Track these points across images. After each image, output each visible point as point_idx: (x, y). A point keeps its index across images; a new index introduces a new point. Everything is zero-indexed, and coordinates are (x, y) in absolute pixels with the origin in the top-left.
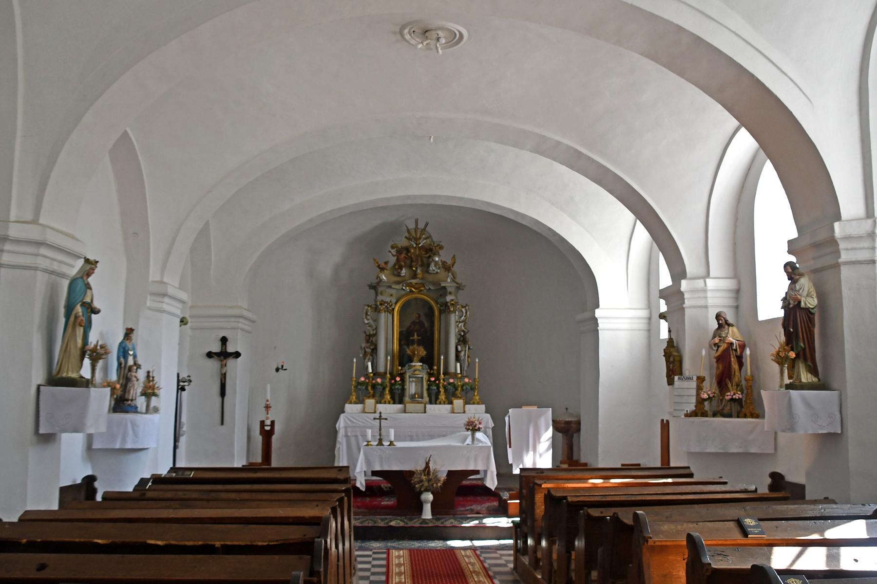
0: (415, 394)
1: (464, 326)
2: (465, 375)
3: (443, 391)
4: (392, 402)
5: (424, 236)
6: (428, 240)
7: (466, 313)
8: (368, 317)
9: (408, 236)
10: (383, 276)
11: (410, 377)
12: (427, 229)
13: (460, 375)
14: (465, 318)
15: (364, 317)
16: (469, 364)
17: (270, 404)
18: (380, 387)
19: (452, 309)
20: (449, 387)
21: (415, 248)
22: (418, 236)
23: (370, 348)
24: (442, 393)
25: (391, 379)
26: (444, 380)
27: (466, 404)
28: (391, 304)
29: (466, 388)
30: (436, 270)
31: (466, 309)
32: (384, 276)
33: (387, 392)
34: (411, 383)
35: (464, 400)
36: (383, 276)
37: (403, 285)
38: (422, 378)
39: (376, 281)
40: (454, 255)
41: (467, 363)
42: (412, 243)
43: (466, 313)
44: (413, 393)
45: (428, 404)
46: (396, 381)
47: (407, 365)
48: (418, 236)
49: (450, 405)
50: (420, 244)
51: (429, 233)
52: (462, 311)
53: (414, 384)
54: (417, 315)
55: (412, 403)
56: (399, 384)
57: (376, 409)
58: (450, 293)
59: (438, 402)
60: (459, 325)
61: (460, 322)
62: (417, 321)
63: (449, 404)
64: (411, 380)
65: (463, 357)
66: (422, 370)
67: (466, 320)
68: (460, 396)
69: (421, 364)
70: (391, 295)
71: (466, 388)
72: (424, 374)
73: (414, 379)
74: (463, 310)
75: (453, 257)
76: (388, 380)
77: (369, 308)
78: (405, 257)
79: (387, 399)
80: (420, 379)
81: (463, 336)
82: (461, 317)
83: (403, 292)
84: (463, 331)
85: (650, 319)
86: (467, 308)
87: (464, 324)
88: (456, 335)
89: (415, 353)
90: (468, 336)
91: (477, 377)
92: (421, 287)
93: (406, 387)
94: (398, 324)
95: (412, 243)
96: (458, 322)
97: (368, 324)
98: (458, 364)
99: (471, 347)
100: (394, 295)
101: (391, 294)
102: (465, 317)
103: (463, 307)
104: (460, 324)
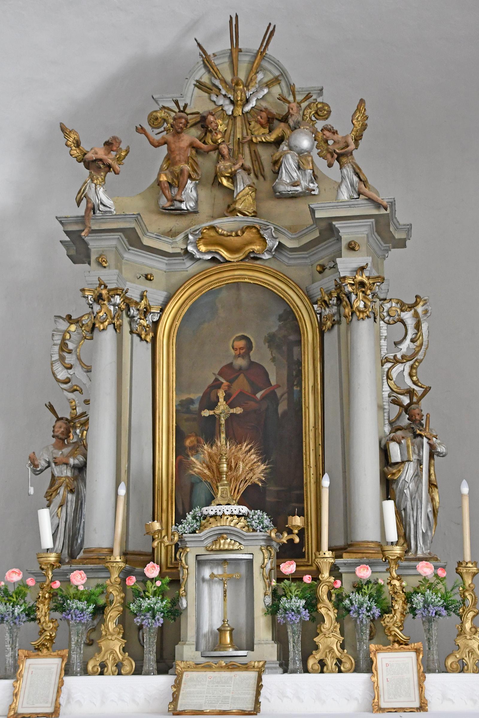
0: (221, 630)
1: (411, 375)
2: (420, 554)
3: (333, 614)
4: (129, 665)
5: (260, 76)
6: (276, 90)
7: (418, 326)
8: (70, 359)
9: (206, 79)
10: (101, 191)
11: (200, 563)
12: (270, 51)
13: (398, 550)
14: (412, 346)
15: (56, 357)
16: (435, 512)
17: (374, 580)
18: (82, 605)
19: (361, 305)
20: (357, 597)
21: (233, 117)
22: (242, 76)
23: (67, 464)
24: (327, 624)
25: (126, 574)
26: (334, 570)
27: (429, 670)
28: (142, 306)
29: (427, 604)
30: (304, 184)
31: (416, 315)
32: (105, 191)
33: (111, 626)
34: (205, 588)
35: (417, 651)
36: (101, 191)
37: (186, 237)
38: (250, 562)
39: (81, 211)
40: (362, 101)
41: (426, 509)
42: (221, 101)
43: (418, 326)
44: (217, 624)
45: (273, 670)
46: (144, 579)
47: (189, 517)
48: (242, 76)
49: (365, 676)
50: (247, 101)
51: (277, 65)
52: (402, 321)
53: (218, 589)
54: (241, 344)
55: (208, 667)
56: (161, 593)
57: (62, 700)
58: (351, 247)
59: (311, 662)
60: (394, 373)
61: (396, 361)
62: (241, 362)
63: (357, 670)
64: (207, 573)
65: (412, 485)
66: (244, 531)
67: (416, 353)
68: (402, 636)
69: (244, 510)
70: (148, 278)
71: (427, 604)
72: (256, 550)
73: (218, 571)
74: (407, 316)
75: (358, 109)
76: (115, 576)
77: (73, 328)
78: (192, 146)
79: (113, 652)
80: (243, 569)
81: (407, 409)
82: (401, 342)
83: (191, 267)
84: (410, 393)
85: (427, 567)
86: (420, 309)
87: (412, 367)
88: (381, 408)
89: (220, 473)
90: (425, 406)
91: (468, 558)
92: (251, 243)
93: (184, 603)
94: (173, 377)
95: (221, 101)
96: (387, 360)
97: (67, 381)
98: (389, 506)
99: (441, 449)
100: (159, 277)
101: (147, 271)
102: (413, 341)
103: (403, 307)
104: (399, 368)
